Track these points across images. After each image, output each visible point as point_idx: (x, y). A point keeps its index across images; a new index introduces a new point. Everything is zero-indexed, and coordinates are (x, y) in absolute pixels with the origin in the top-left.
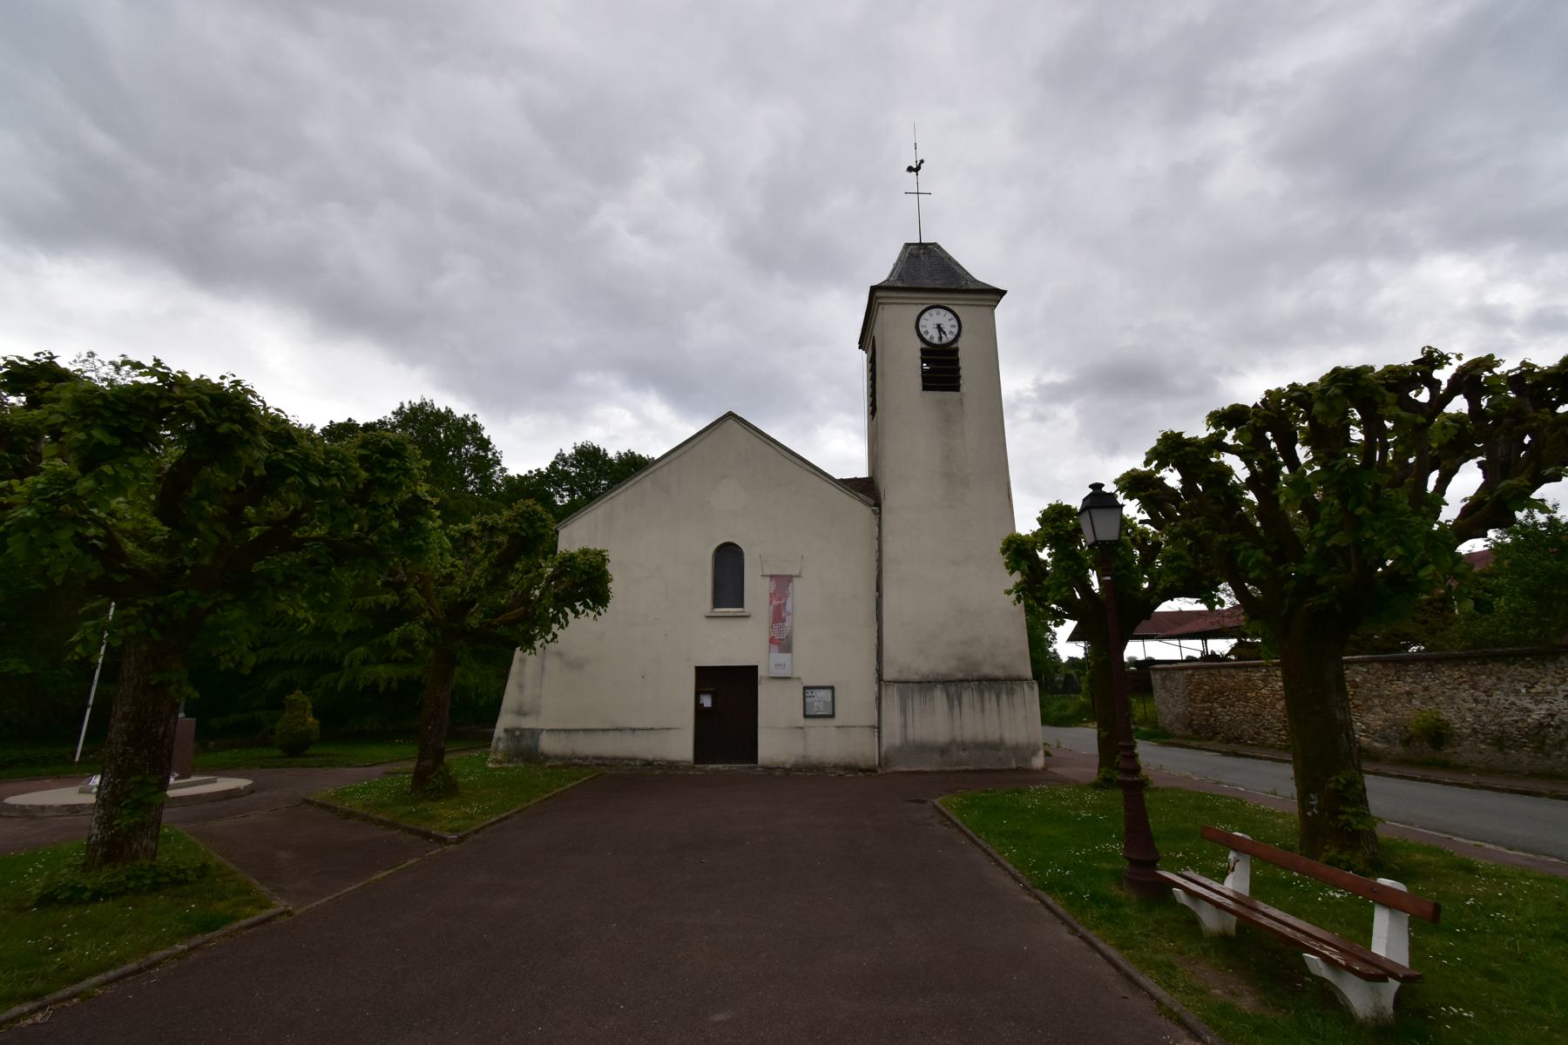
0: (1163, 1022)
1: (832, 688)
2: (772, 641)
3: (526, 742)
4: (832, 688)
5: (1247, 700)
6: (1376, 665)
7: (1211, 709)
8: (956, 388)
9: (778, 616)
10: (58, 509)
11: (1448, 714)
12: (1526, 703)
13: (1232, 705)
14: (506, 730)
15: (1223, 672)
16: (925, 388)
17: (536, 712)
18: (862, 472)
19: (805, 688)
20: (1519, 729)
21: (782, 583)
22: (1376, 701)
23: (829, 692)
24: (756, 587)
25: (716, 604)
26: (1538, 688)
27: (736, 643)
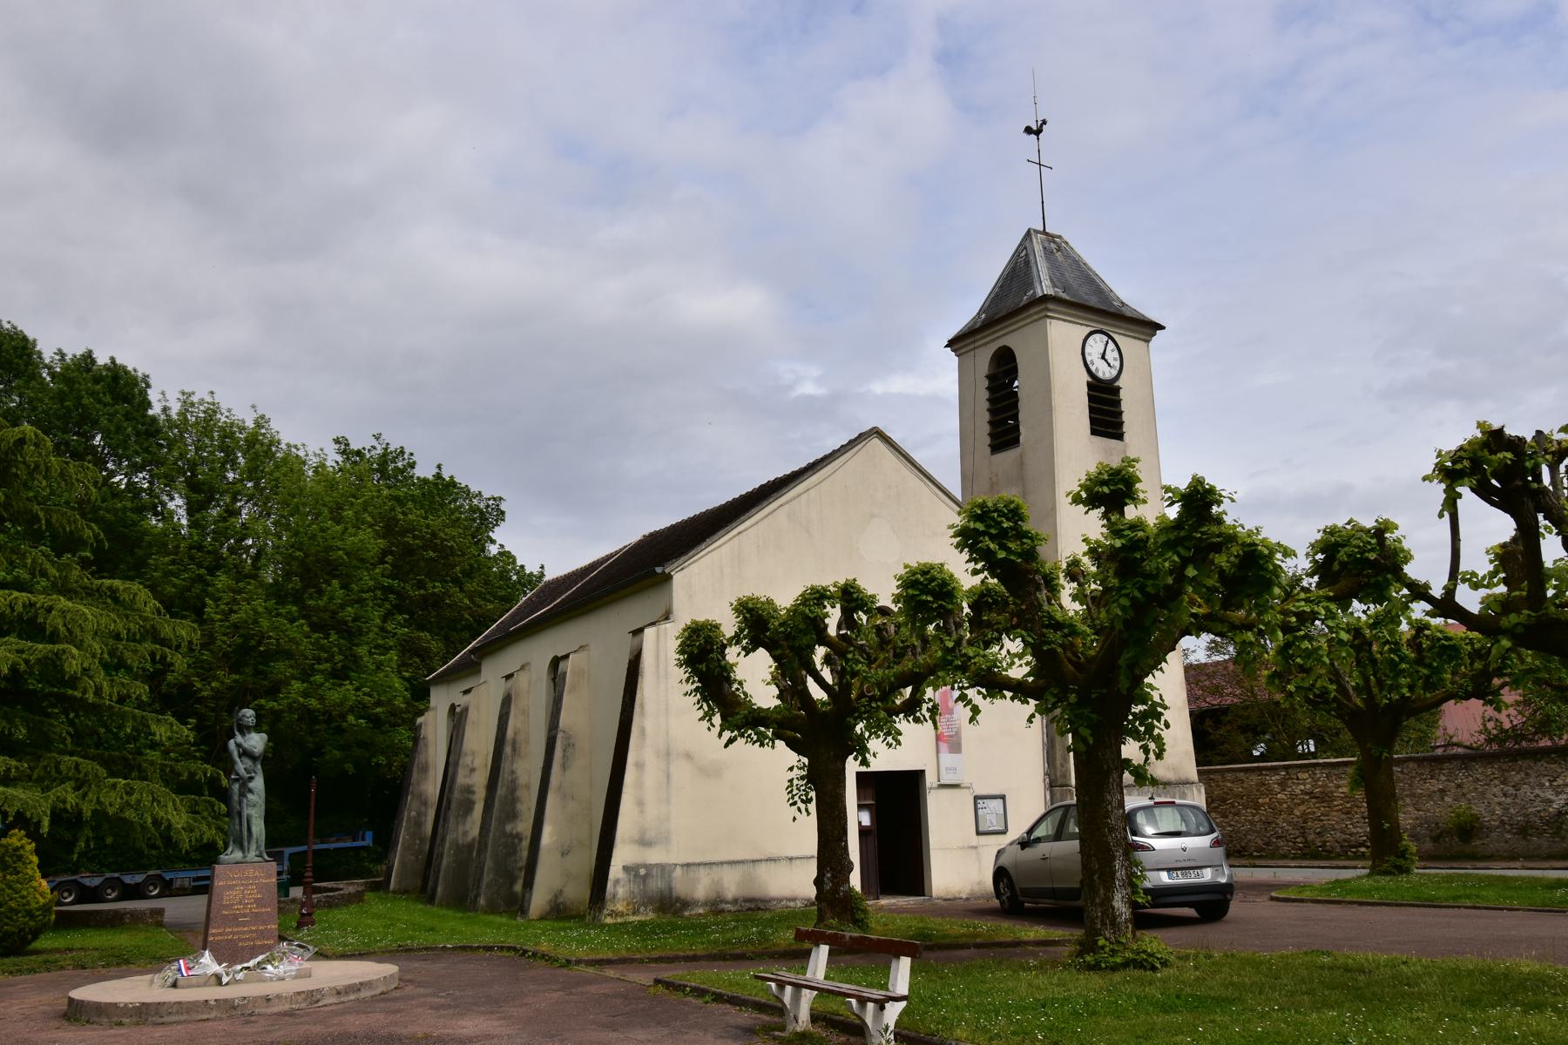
1: (1003, 797)
3: (656, 884)
4: (1003, 797)
5: (1257, 807)
6: (1411, 765)
11: (1479, 809)
12: (1549, 794)
13: (1237, 814)
14: (626, 869)
15: (1229, 776)
16: (1094, 432)
17: (664, 839)
19: (976, 798)
20: (1541, 818)
22: (1408, 800)
26: (1560, 781)
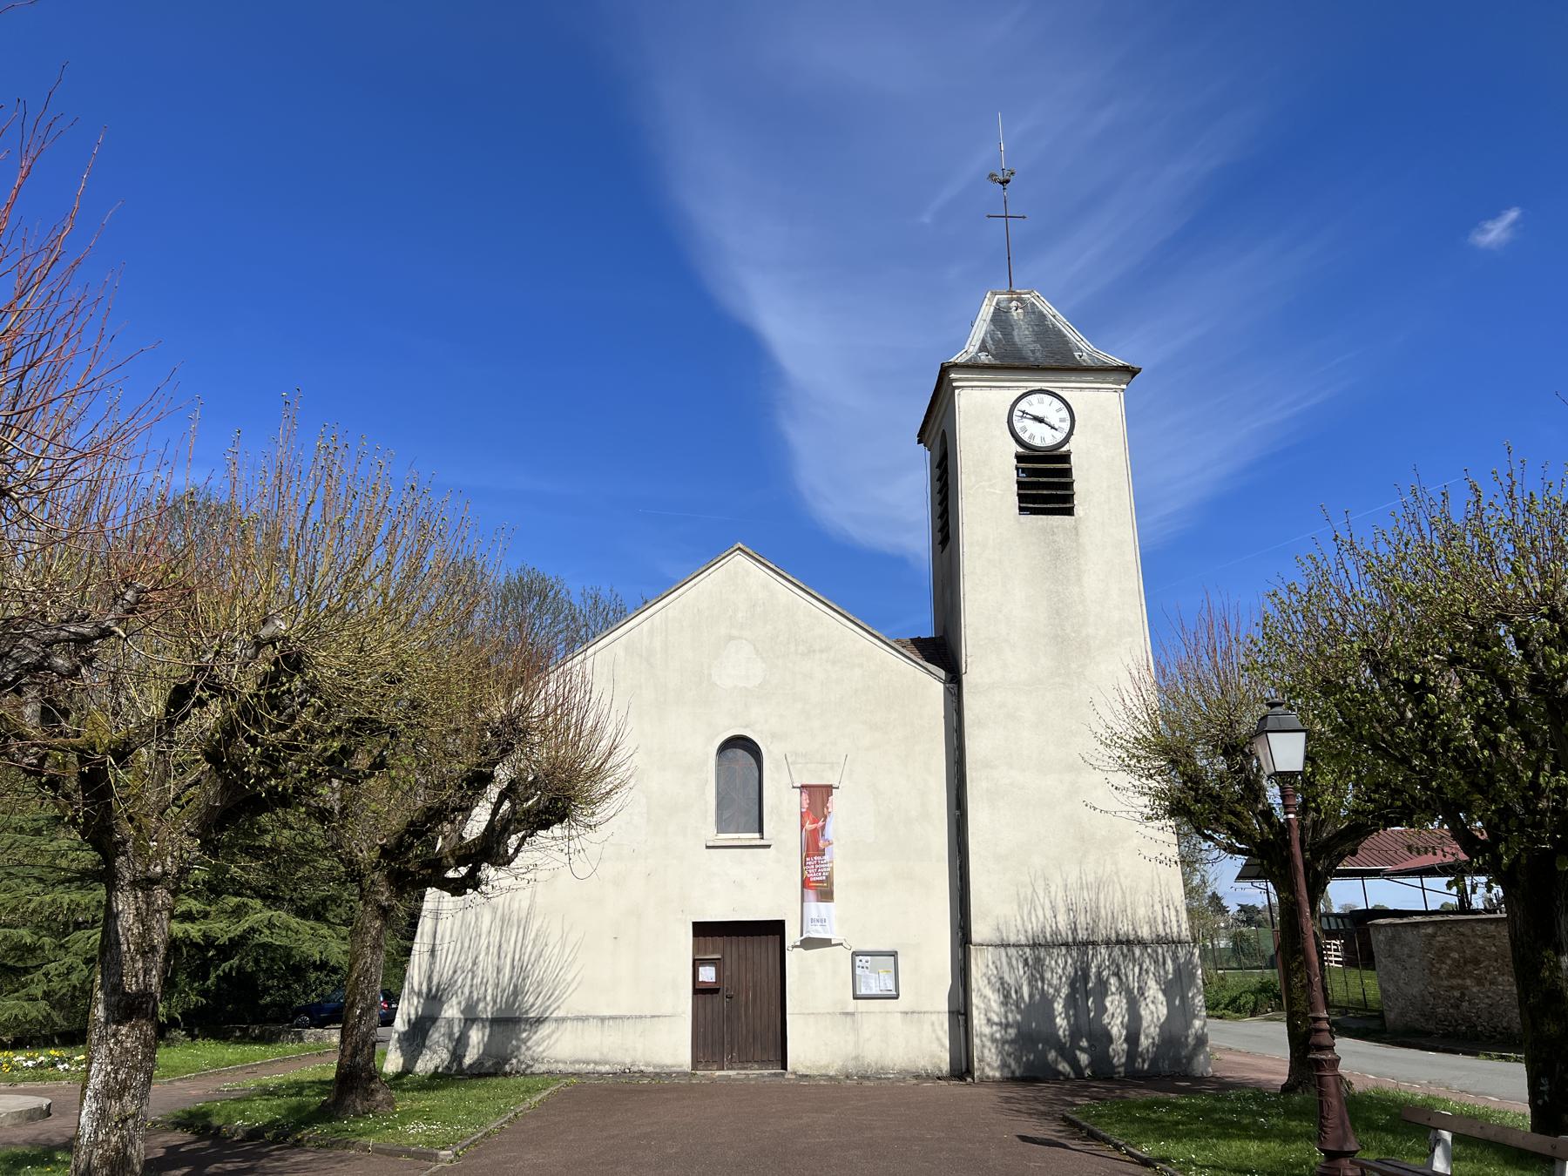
1: (894, 954)
2: (805, 883)
7: (1463, 989)
9: (813, 846)
10: (253, 787)
18: (928, 632)
19: (855, 954)
23: (863, 991)
25: (722, 826)
27: (756, 886)
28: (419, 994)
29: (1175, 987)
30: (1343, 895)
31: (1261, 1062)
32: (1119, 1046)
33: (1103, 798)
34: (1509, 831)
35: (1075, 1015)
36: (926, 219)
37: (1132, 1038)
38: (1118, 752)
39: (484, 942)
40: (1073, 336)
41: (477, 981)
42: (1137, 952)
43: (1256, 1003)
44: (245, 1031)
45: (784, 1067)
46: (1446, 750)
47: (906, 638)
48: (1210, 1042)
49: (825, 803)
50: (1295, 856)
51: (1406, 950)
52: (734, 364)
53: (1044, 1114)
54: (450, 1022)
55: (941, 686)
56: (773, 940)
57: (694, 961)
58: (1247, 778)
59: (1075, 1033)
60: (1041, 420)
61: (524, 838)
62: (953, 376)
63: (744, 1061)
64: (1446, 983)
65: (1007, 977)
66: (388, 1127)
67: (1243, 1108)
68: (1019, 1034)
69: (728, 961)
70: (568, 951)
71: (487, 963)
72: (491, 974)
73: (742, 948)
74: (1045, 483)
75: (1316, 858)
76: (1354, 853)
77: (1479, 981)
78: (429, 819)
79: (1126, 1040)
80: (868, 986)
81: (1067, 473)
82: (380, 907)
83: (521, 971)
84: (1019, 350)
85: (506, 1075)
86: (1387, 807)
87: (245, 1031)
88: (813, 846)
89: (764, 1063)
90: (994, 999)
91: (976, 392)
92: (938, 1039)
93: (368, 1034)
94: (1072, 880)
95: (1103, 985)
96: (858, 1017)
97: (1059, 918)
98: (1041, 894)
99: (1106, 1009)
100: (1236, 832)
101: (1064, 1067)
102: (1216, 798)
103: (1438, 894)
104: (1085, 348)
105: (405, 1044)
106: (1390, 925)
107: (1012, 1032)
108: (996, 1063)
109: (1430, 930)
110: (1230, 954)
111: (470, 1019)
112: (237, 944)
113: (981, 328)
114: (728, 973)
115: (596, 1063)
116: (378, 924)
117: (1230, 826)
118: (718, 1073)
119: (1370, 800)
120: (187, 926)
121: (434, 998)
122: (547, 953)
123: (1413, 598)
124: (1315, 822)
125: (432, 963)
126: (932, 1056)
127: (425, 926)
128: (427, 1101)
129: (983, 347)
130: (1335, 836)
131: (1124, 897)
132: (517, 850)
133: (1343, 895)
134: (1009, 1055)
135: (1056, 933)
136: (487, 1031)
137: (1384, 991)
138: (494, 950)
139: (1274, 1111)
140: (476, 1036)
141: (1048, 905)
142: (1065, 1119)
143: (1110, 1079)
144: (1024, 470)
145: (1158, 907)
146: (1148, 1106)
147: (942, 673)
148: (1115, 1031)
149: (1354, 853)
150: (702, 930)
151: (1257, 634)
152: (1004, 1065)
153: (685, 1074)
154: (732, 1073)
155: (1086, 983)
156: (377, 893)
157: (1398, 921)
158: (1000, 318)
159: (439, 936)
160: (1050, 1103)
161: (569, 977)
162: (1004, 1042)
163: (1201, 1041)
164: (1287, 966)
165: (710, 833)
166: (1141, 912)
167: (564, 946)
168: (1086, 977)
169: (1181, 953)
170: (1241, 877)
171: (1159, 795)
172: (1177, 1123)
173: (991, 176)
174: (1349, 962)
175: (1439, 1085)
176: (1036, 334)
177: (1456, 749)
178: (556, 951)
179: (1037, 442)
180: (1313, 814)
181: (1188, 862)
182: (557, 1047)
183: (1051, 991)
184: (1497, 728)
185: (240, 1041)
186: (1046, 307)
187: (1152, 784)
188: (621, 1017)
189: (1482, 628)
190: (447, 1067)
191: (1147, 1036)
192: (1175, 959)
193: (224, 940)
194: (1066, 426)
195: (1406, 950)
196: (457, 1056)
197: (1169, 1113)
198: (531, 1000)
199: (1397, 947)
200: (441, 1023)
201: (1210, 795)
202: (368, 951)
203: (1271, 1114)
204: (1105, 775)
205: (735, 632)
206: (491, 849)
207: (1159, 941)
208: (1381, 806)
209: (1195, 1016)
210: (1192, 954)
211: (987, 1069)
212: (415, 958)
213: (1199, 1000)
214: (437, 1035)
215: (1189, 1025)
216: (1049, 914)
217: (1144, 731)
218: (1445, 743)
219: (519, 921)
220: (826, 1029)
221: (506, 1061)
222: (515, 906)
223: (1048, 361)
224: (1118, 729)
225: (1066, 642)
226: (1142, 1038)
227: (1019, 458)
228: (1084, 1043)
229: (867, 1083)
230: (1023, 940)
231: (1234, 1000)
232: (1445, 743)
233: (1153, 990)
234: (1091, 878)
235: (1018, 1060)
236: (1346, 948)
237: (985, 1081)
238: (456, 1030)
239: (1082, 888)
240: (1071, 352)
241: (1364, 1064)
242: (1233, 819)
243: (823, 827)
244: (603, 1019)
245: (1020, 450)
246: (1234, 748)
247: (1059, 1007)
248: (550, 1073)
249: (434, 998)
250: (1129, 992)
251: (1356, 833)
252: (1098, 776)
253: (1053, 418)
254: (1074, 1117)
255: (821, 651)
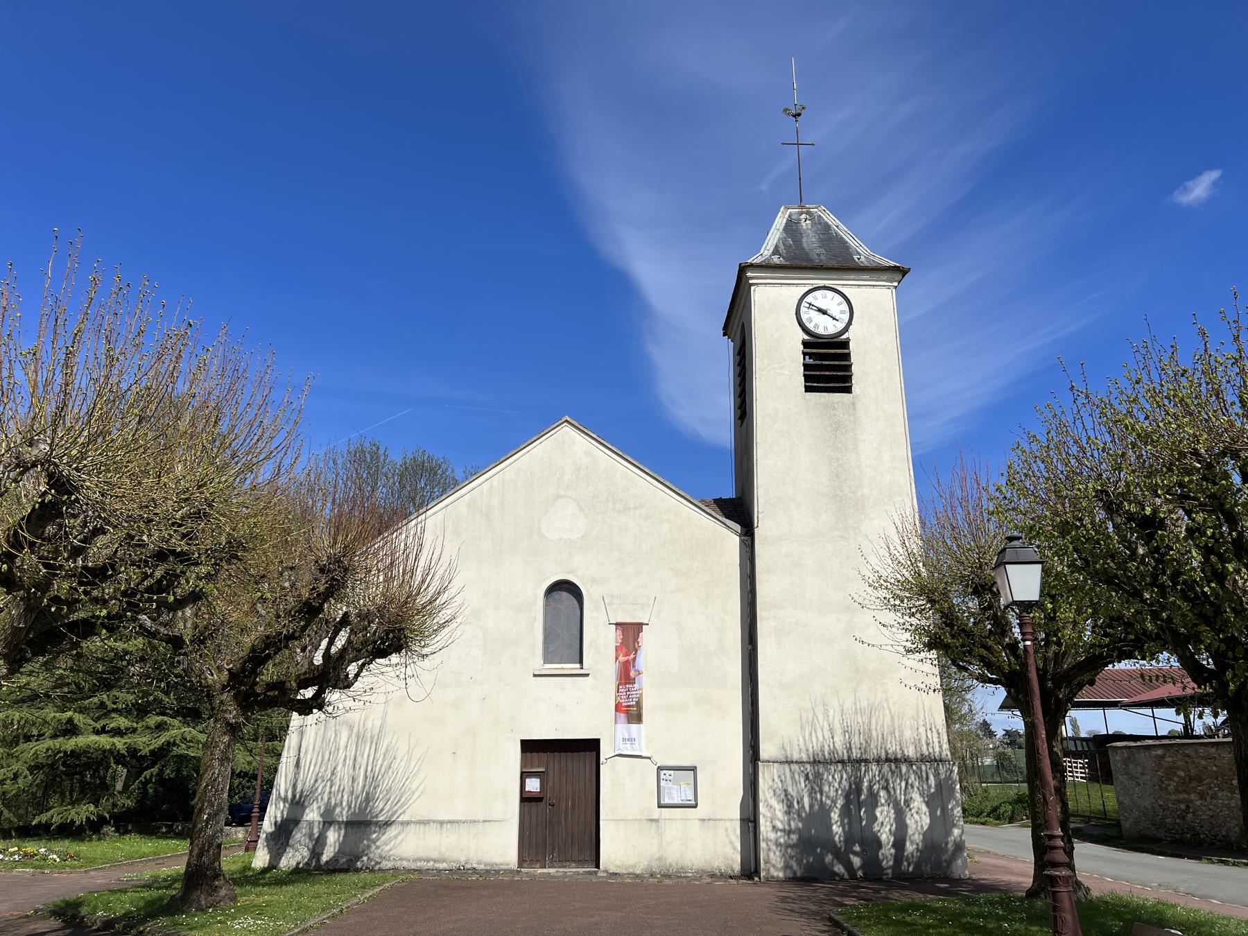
0: (118, 895)
1: (694, 769)
2: (618, 707)
7: (1188, 803)
8: (848, 390)
9: (626, 676)
18: (729, 493)
19: (660, 769)
21: (630, 633)
23: (666, 801)
24: (600, 640)
25: (548, 657)
27: (575, 709)
28: (285, 800)
29: (937, 801)
30: (1085, 722)
31: (1013, 865)
32: (888, 851)
33: (873, 633)
34: (1236, 659)
35: (850, 824)
36: (764, 187)
37: (899, 844)
38: (883, 593)
39: (341, 755)
40: (853, 242)
41: (335, 788)
42: (904, 769)
43: (1013, 812)
44: (170, 828)
45: (598, 867)
46: (1175, 584)
47: (710, 499)
48: (967, 845)
49: (636, 638)
50: (1045, 687)
51: (1139, 769)
52: (608, 301)
53: (814, 913)
54: (311, 824)
55: (737, 539)
56: (589, 756)
57: (522, 773)
58: (995, 615)
59: (849, 839)
60: (824, 312)
61: (363, 665)
62: (749, 274)
63: (563, 861)
64: (1173, 797)
65: (790, 790)
66: (220, 922)
67: (989, 913)
68: (800, 839)
69: (551, 773)
70: (413, 764)
71: (344, 773)
72: (346, 782)
73: (563, 763)
74: (828, 366)
75: (1058, 686)
76: (1092, 683)
77: (1202, 796)
78: (267, 646)
79: (894, 846)
80: (671, 797)
81: (847, 357)
82: (228, 724)
83: (373, 780)
84: (807, 254)
85: (357, 870)
86: (1121, 640)
87: (170, 828)
88: (626, 676)
89: (580, 862)
90: (779, 809)
91: (768, 288)
92: (731, 843)
93: (214, 837)
94: (848, 705)
95: (873, 797)
96: (662, 823)
97: (836, 739)
98: (821, 718)
99: (876, 818)
100: (988, 665)
101: (839, 868)
102: (969, 634)
103: (1168, 721)
104: (863, 252)
105: (272, 843)
106: (1126, 747)
107: (794, 837)
108: (780, 865)
109: (1160, 752)
110: (994, 770)
111: (328, 822)
112: (159, 754)
113: (775, 235)
114: (550, 784)
115: (435, 861)
116: (226, 739)
117: (982, 659)
118: (540, 871)
119: (1106, 635)
120: (115, 740)
121: (298, 803)
122: (394, 766)
123: (1145, 438)
124: (1056, 654)
125: (297, 774)
126: (726, 858)
127: (291, 740)
128: (266, 896)
129: (776, 251)
130: (1074, 667)
131: (893, 720)
132: (357, 675)
133: (1085, 722)
134: (791, 857)
135: (833, 751)
136: (343, 832)
137: (1120, 803)
138: (350, 762)
139: (1018, 916)
140: (333, 837)
141: (826, 726)
142: (830, 919)
143: (879, 880)
144: (811, 355)
145: (922, 730)
146: (904, 909)
147: (738, 528)
148: (884, 837)
149: (1092, 683)
150: (529, 747)
151: (1003, 481)
152: (787, 867)
153: (511, 871)
154: (552, 871)
155: (859, 796)
156: (225, 712)
157: (1132, 744)
158: (791, 227)
159: (303, 750)
160: (820, 903)
161: (414, 787)
162: (788, 846)
163: (959, 847)
164: (1034, 785)
165: (538, 664)
166: (908, 734)
167: (410, 760)
168: (859, 791)
169: (942, 769)
170: (1002, 707)
171: (917, 630)
172: (929, 927)
173: (786, 110)
174: (1092, 778)
175: (1167, 887)
176: (821, 240)
177: (1185, 582)
178: (403, 764)
179: (821, 331)
180: (1054, 648)
181: (952, 696)
182: (402, 847)
183: (829, 802)
184: (1223, 560)
185: (165, 836)
186: (830, 219)
187: (914, 621)
188: (457, 822)
189: (1210, 466)
190: (307, 864)
191: (912, 843)
192: (937, 775)
193: (146, 751)
194: (846, 317)
195: (1139, 769)
196: (316, 853)
197: (923, 916)
198: (381, 806)
199: (1131, 766)
200: (303, 825)
201: (963, 630)
202: (216, 763)
203: (1014, 919)
204: (873, 613)
205: (562, 492)
206: (331, 676)
207: (923, 759)
208: (1115, 640)
209: (954, 825)
210: (952, 771)
211: (772, 870)
212: (282, 768)
213: (958, 811)
214: (299, 836)
215: (948, 833)
216: (827, 734)
217: (907, 575)
218: (1175, 576)
219: (372, 738)
220: (634, 833)
221: (358, 858)
222: (369, 724)
223: (836, 263)
224: (884, 574)
225: (844, 500)
226: (908, 844)
227: (806, 344)
228: (857, 848)
229: (667, 881)
230: (805, 758)
231: (995, 809)
232: (1175, 576)
233: (918, 802)
234: (864, 704)
235: (799, 862)
236: (1091, 766)
237: (770, 880)
238: (316, 831)
239: (856, 712)
240: (851, 255)
241: (1101, 869)
242: (985, 653)
243: (634, 659)
244: (442, 823)
245: (806, 337)
246: (982, 586)
247: (835, 816)
248: (395, 869)
249: (298, 803)
250: (896, 804)
251: (1094, 663)
252: (868, 616)
253: (834, 311)
254: (838, 918)
255: (635, 508)
